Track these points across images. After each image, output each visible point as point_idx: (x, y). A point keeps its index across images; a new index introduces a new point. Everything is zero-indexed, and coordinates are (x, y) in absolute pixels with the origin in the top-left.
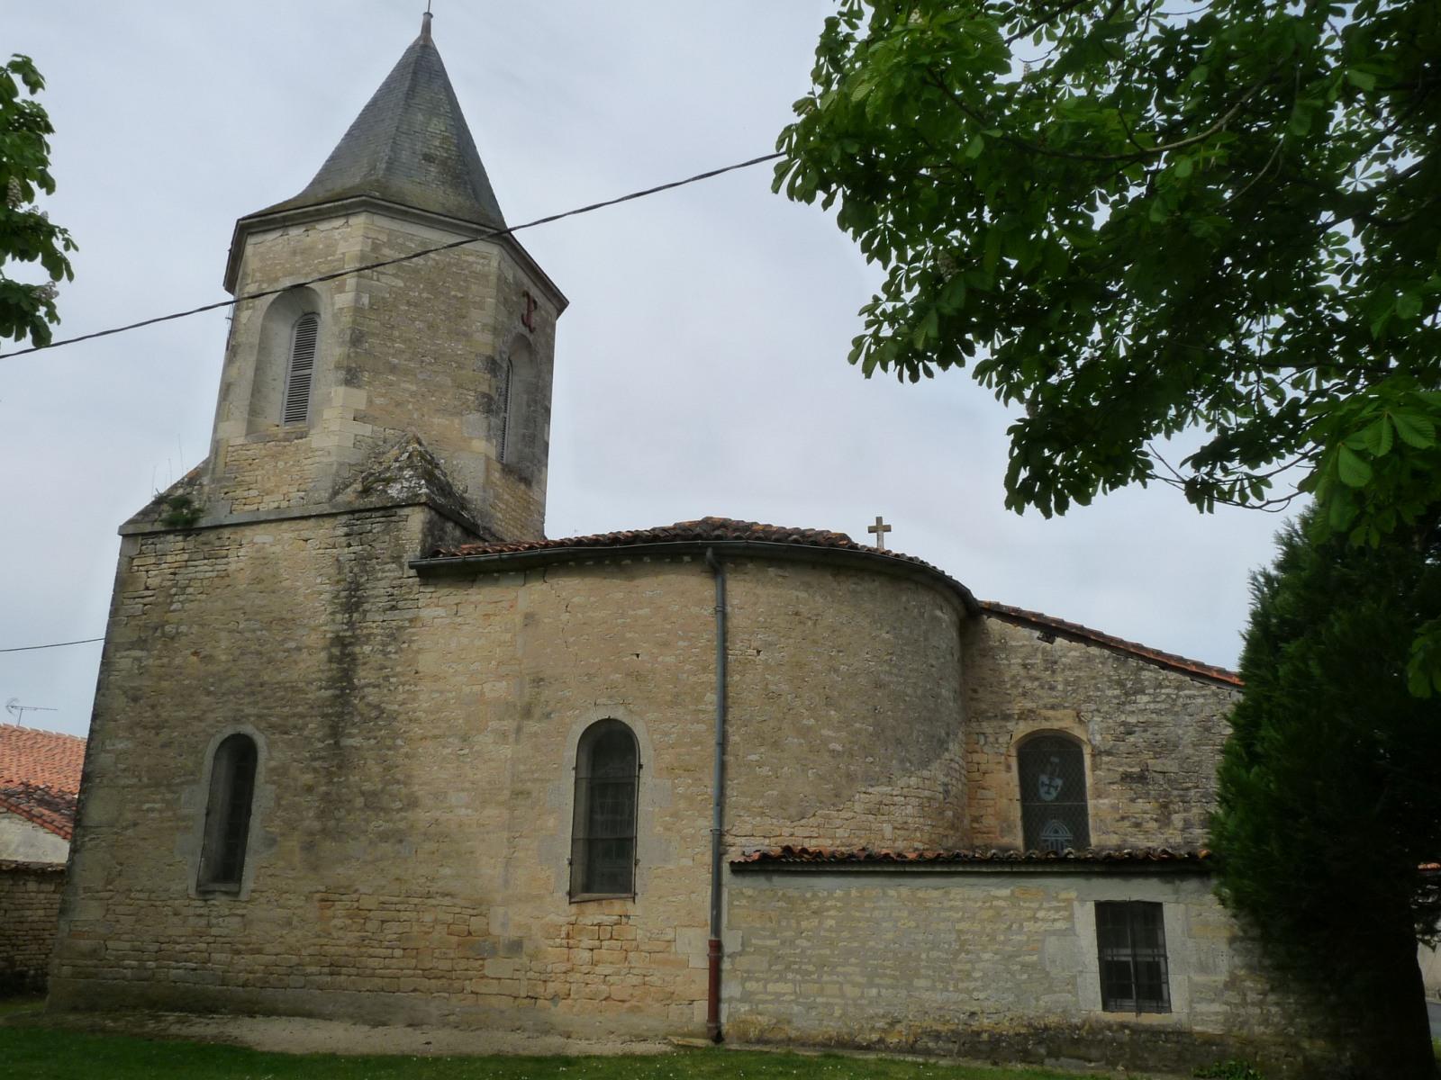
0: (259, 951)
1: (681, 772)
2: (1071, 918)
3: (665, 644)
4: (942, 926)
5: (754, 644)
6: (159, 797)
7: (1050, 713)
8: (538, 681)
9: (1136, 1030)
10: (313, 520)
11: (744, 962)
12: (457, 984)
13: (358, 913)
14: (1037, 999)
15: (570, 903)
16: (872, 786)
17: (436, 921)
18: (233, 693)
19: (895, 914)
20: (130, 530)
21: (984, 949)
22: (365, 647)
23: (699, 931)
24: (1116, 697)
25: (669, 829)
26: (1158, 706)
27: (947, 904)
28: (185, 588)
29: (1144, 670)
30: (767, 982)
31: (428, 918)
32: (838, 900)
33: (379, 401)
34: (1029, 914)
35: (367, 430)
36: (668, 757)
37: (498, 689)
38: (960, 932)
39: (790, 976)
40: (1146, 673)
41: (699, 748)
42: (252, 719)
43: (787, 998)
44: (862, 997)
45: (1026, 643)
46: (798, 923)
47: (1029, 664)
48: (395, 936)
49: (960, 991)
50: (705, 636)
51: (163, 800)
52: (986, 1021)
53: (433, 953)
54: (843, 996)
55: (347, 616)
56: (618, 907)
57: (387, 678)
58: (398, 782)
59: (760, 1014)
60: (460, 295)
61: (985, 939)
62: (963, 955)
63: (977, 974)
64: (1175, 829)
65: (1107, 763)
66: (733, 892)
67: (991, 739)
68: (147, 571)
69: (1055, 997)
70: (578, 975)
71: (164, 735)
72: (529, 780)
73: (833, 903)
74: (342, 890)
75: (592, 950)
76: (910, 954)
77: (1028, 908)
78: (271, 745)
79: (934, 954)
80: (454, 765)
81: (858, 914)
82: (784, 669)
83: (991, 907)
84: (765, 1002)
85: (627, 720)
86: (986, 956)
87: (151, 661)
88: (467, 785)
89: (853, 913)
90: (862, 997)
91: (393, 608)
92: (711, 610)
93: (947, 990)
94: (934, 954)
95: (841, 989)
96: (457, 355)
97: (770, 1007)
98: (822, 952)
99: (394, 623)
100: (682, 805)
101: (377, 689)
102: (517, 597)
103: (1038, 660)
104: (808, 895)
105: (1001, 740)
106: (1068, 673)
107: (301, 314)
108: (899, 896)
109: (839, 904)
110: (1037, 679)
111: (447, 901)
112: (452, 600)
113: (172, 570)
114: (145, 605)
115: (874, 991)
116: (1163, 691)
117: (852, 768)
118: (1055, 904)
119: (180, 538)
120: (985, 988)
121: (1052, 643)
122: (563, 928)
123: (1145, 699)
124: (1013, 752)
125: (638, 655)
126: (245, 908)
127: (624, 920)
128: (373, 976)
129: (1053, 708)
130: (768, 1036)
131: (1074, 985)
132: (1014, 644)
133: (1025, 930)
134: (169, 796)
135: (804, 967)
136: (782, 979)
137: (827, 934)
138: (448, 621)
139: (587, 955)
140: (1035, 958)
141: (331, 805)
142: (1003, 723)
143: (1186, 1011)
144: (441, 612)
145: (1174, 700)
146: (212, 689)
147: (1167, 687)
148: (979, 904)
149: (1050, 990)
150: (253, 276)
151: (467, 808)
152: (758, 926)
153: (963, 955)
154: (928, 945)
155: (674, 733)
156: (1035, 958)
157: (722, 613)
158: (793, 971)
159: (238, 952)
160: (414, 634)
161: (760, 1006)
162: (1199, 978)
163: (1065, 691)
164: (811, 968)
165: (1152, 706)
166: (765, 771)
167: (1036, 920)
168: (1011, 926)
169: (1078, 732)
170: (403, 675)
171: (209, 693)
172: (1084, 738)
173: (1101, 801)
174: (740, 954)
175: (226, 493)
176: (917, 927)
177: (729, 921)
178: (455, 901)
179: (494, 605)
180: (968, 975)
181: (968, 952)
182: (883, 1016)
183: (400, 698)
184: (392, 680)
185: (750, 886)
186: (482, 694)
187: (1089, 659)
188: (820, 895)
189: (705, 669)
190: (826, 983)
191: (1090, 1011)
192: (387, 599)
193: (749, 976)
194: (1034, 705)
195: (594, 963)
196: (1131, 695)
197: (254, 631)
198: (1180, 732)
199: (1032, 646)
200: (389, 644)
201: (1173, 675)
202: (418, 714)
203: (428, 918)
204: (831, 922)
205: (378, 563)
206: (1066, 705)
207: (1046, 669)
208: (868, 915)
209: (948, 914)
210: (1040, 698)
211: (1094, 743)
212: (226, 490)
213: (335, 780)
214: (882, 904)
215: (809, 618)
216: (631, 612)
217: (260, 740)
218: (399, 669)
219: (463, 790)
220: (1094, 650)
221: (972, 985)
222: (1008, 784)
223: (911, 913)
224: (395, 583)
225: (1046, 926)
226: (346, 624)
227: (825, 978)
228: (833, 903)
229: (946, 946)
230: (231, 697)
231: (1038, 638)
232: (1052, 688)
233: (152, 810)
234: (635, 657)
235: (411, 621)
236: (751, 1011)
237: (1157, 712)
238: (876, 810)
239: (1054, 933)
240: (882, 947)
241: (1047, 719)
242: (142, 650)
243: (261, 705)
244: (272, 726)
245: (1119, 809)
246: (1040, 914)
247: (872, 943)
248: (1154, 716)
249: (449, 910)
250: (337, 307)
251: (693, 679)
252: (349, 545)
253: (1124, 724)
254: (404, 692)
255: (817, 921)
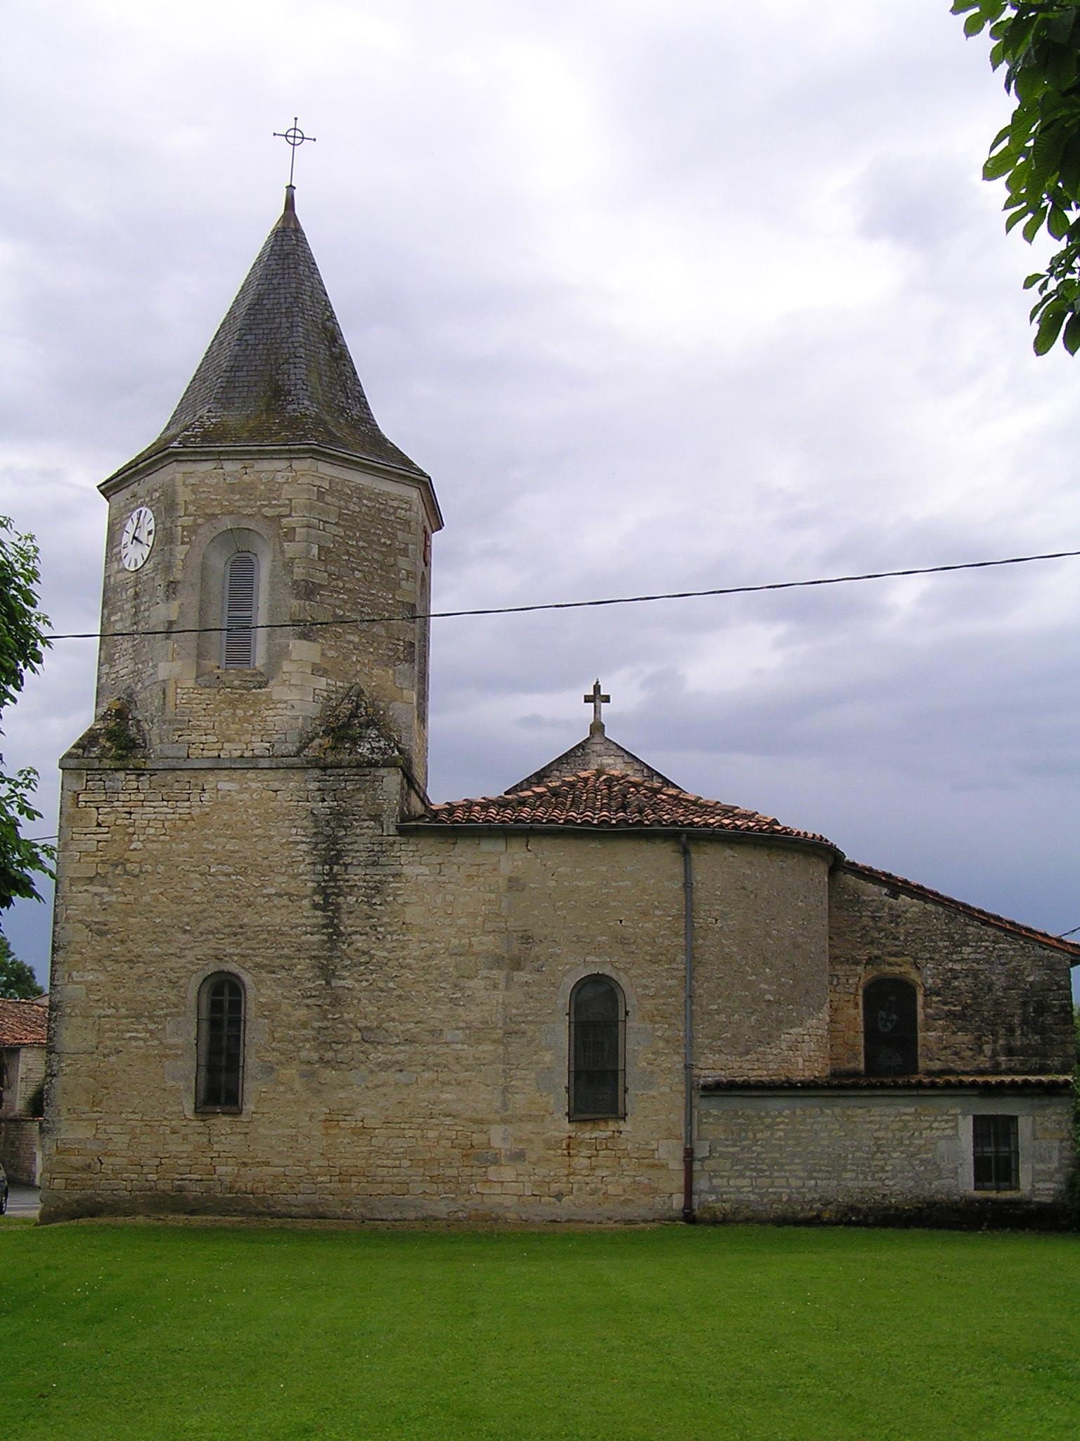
0: (267, 1164)
1: (660, 1019)
2: (955, 1127)
3: (645, 914)
4: (864, 1135)
5: (714, 914)
6: (141, 1027)
7: (893, 959)
8: (527, 939)
9: (995, 1202)
10: (281, 771)
11: (710, 1164)
12: (463, 1188)
13: (363, 1130)
14: (930, 1184)
15: (569, 1122)
16: (791, 1028)
17: (440, 1138)
18: (212, 932)
19: (830, 1127)
20: (72, 763)
21: (895, 1151)
22: (349, 898)
23: (675, 1142)
24: (946, 947)
25: (651, 1064)
26: (978, 956)
27: (868, 1119)
28: (145, 828)
29: (969, 925)
30: (729, 1178)
31: (432, 1134)
32: (786, 1117)
33: (331, 654)
34: (927, 1125)
35: (322, 683)
36: (649, 1005)
37: (486, 943)
38: (877, 1139)
39: (748, 1173)
40: (971, 928)
41: (673, 999)
42: (236, 958)
43: (746, 1189)
44: (804, 1186)
45: (875, 898)
46: (755, 1134)
47: (877, 917)
48: (402, 1150)
49: (876, 1180)
50: (676, 907)
51: (148, 1031)
52: (893, 1201)
53: (439, 1163)
54: (789, 1186)
55: (327, 867)
56: (612, 1126)
57: (374, 927)
58: (393, 1020)
59: (724, 1202)
60: (389, 542)
61: (895, 1143)
62: (879, 1154)
63: (887, 1168)
64: (985, 1056)
65: (936, 1002)
66: (702, 1113)
67: (843, 980)
68: (98, 808)
69: (943, 1182)
70: (579, 1177)
71: (140, 969)
72: (523, 1022)
73: (782, 1119)
74: (345, 1112)
75: (590, 1158)
76: (840, 1155)
77: (927, 1121)
78: (259, 982)
79: (858, 1154)
80: (448, 1007)
81: (802, 1127)
82: (734, 934)
83: (900, 1121)
84: (730, 1193)
85: (614, 976)
86: (895, 1155)
87: (114, 898)
88: (461, 1025)
89: (798, 1126)
90: (804, 1186)
91: (375, 864)
92: (680, 885)
93: (867, 1180)
94: (858, 1154)
95: (787, 1181)
96: (388, 604)
97: (733, 1197)
98: (774, 1155)
99: (378, 877)
100: (661, 1044)
101: (364, 937)
102: (499, 860)
103: (884, 913)
104: (763, 1114)
105: (850, 981)
106: (909, 926)
107: (235, 550)
108: (833, 1113)
109: (786, 1121)
110: (883, 930)
111: (448, 1121)
112: (435, 860)
113: (127, 809)
114: (99, 841)
115: (813, 1182)
116: (983, 944)
117: (780, 1014)
118: (945, 1117)
119: (133, 777)
120: (894, 1177)
121: (897, 899)
122: (564, 1142)
123: (969, 950)
124: (861, 992)
125: (621, 921)
126: (248, 1127)
127: (616, 1134)
128: (383, 1182)
129: (895, 955)
130: (730, 1216)
131: (956, 1173)
132: (865, 898)
133: (924, 1136)
134: (152, 1027)
135: (759, 1167)
136: (742, 1176)
137: (778, 1142)
138: (432, 879)
139: (587, 1162)
140: (930, 1155)
141: (325, 1041)
142: (853, 967)
143: (1029, 1188)
144: (425, 870)
145: (991, 952)
146: (188, 928)
147: (987, 941)
148: (892, 1119)
149: (940, 1177)
150: (186, 509)
151: (463, 1044)
152: (723, 1137)
153: (879, 1154)
154: (854, 1149)
155: (653, 987)
156: (930, 1155)
157: (688, 886)
158: (751, 1170)
159: (245, 1164)
160: (399, 888)
161: (724, 1196)
162: (1040, 1167)
163: (906, 940)
164: (765, 1167)
165: (972, 956)
166: (723, 1018)
167: (931, 1128)
168: (913, 1134)
169: (914, 976)
170: (391, 925)
171: (186, 932)
172: (919, 981)
173: (930, 1034)
174: (707, 1158)
175: (179, 736)
176: (846, 1135)
177: (699, 1134)
178: (457, 1121)
179: (476, 867)
180: (883, 1169)
181: (882, 1153)
182: (820, 1200)
183: (389, 945)
184: (379, 929)
185: (713, 1108)
186: (471, 945)
187: (926, 913)
188: (772, 1113)
189: (677, 935)
190: (776, 1177)
191: (966, 1191)
192: (366, 854)
193: (715, 1174)
194: (880, 952)
195: (593, 1168)
196: (959, 946)
197: (228, 875)
198: (994, 978)
199: (881, 901)
200: (374, 897)
201: (991, 931)
202: (408, 961)
203: (432, 1134)
204: (781, 1134)
205: (355, 820)
206: (906, 953)
207: (892, 922)
208: (809, 1128)
209: (869, 1126)
210: (885, 946)
211: (927, 986)
212: (180, 733)
213: (330, 1016)
214: (820, 1119)
215: (752, 892)
216: (614, 884)
217: (247, 978)
218: (385, 919)
219: (458, 1029)
220: (930, 907)
221: (884, 1176)
222: (856, 1019)
223: (841, 1126)
224: (374, 840)
225: (939, 1133)
226: (327, 875)
227: (776, 1174)
228: (782, 1119)
229: (867, 1149)
230: (211, 937)
231: (886, 894)
232: (896, 939)
233: (135, 1039)
234: (619, 923)
235: (394, 876)
236: (717, 1201)
237: (977, 961)
238: (793, 1047)
239: (944, 1137)
240: (819, 1150)
241: (890, 964)
242: (103, 886)
243: (244, 945)
244: (258, 966)
245: (943, 1040)
246: (935, 1125)
247: (811, 1148)
248: (975, 964)
249: (451, 1128)
250: (288, 555)
251: (667, 942)
252: (323, 800)
253: (951, 970)
254: (392, 941)
255: (769, 1133)
